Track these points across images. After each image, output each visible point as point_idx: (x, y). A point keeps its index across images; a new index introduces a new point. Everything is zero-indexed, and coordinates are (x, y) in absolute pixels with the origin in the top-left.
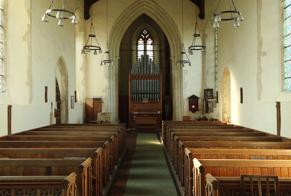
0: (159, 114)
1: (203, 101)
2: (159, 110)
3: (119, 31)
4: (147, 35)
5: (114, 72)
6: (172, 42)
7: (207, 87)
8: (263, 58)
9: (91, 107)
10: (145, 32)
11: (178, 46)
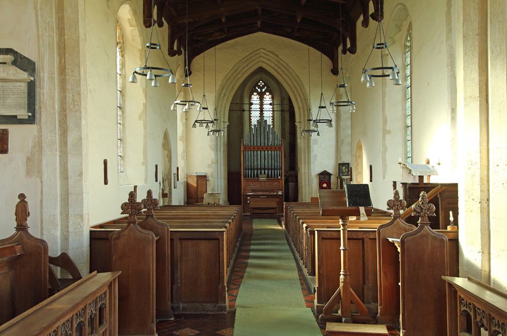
0: (280, 195)
1: (337, 178)
2: (281, 190)
3: (229, 90)
4: (263, 87)
5: (222, 142)
6: (298, 103)
7: (343, 161)
8: (387, 136)
9: (194, 186)
10: (261, 83)
11: (305, 108)
